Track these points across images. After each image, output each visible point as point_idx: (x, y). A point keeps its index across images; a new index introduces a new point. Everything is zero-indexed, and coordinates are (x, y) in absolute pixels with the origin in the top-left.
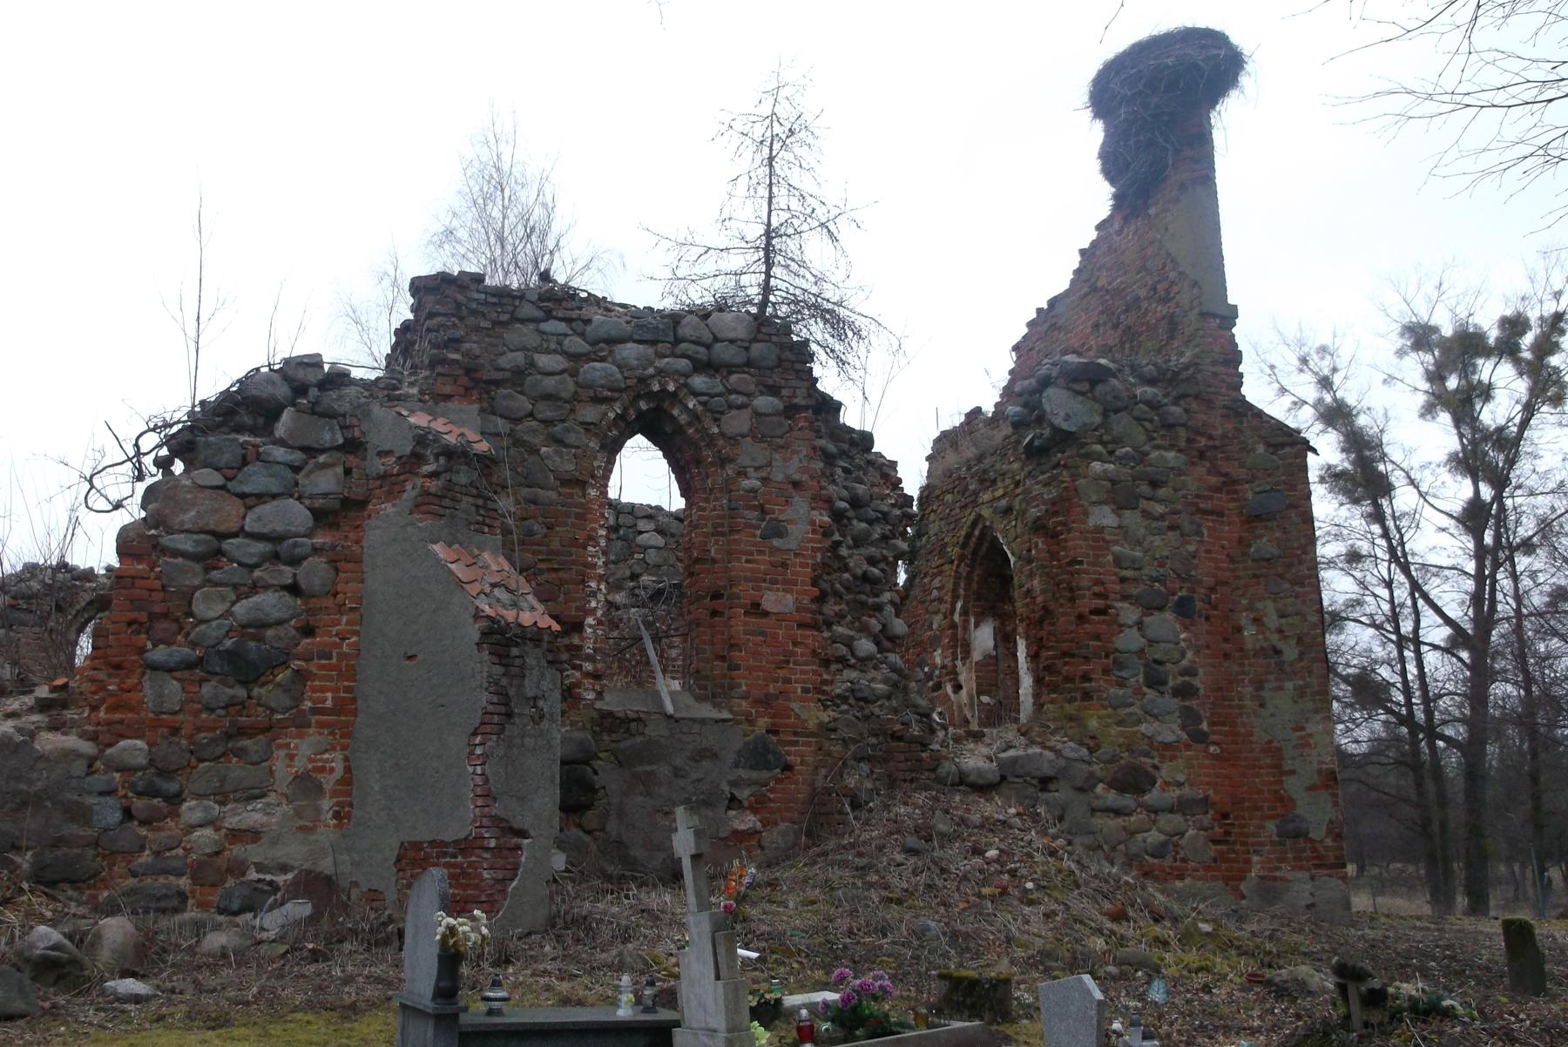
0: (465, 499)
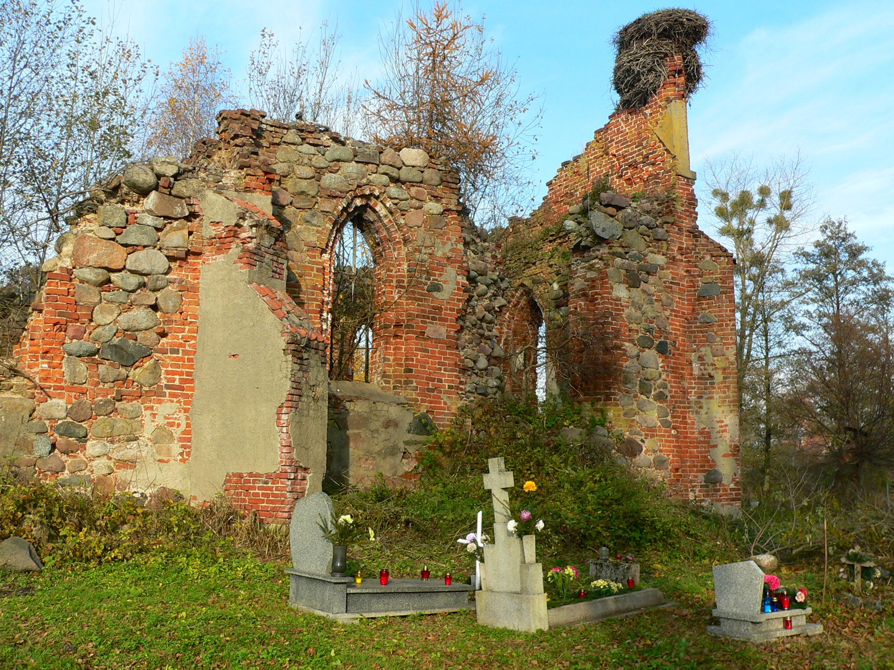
0: (267, 256)
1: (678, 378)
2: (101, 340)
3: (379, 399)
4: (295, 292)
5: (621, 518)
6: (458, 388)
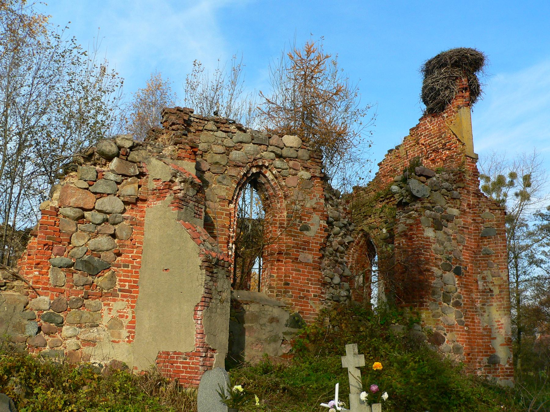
0: (191, 202)
1: (468, 291)
2: (76, 257)
3: (266, 303)
4: (210, 229)
5: (435, 388)
6: (320, 296)
